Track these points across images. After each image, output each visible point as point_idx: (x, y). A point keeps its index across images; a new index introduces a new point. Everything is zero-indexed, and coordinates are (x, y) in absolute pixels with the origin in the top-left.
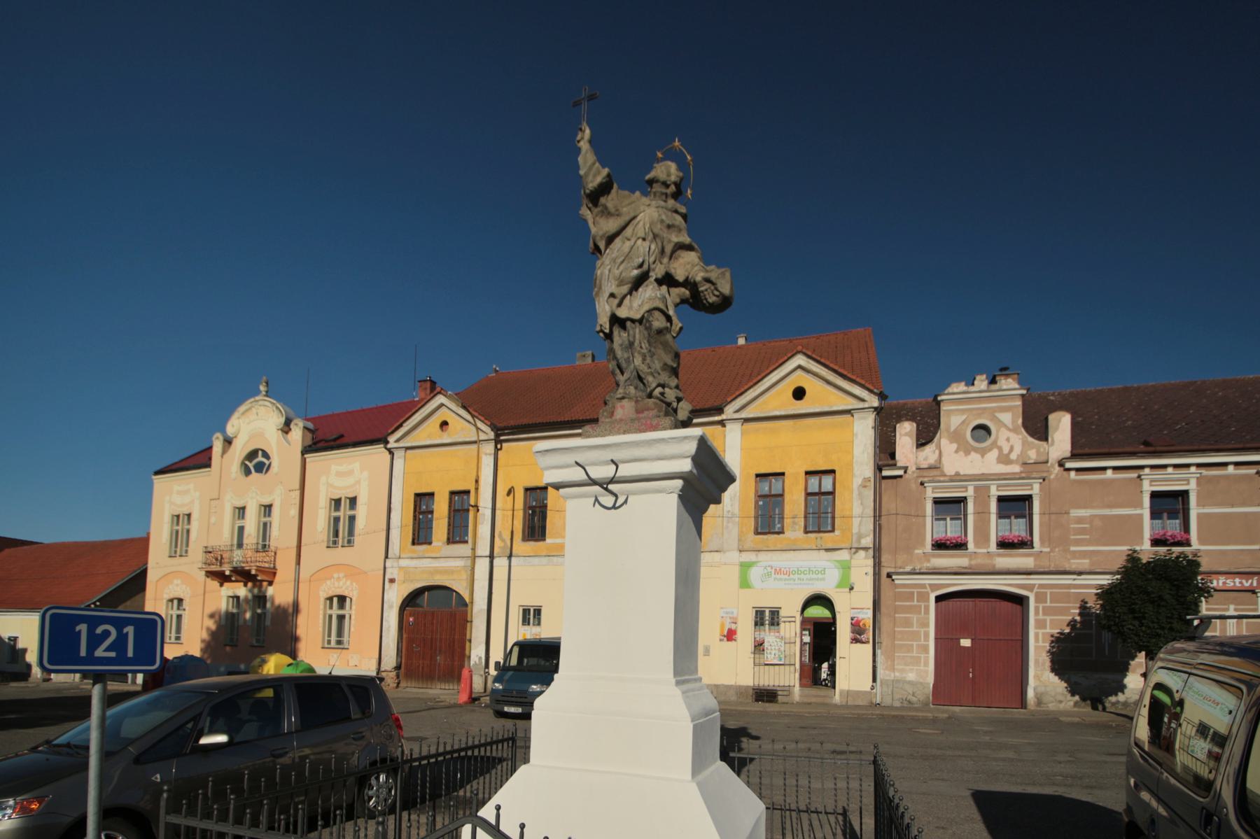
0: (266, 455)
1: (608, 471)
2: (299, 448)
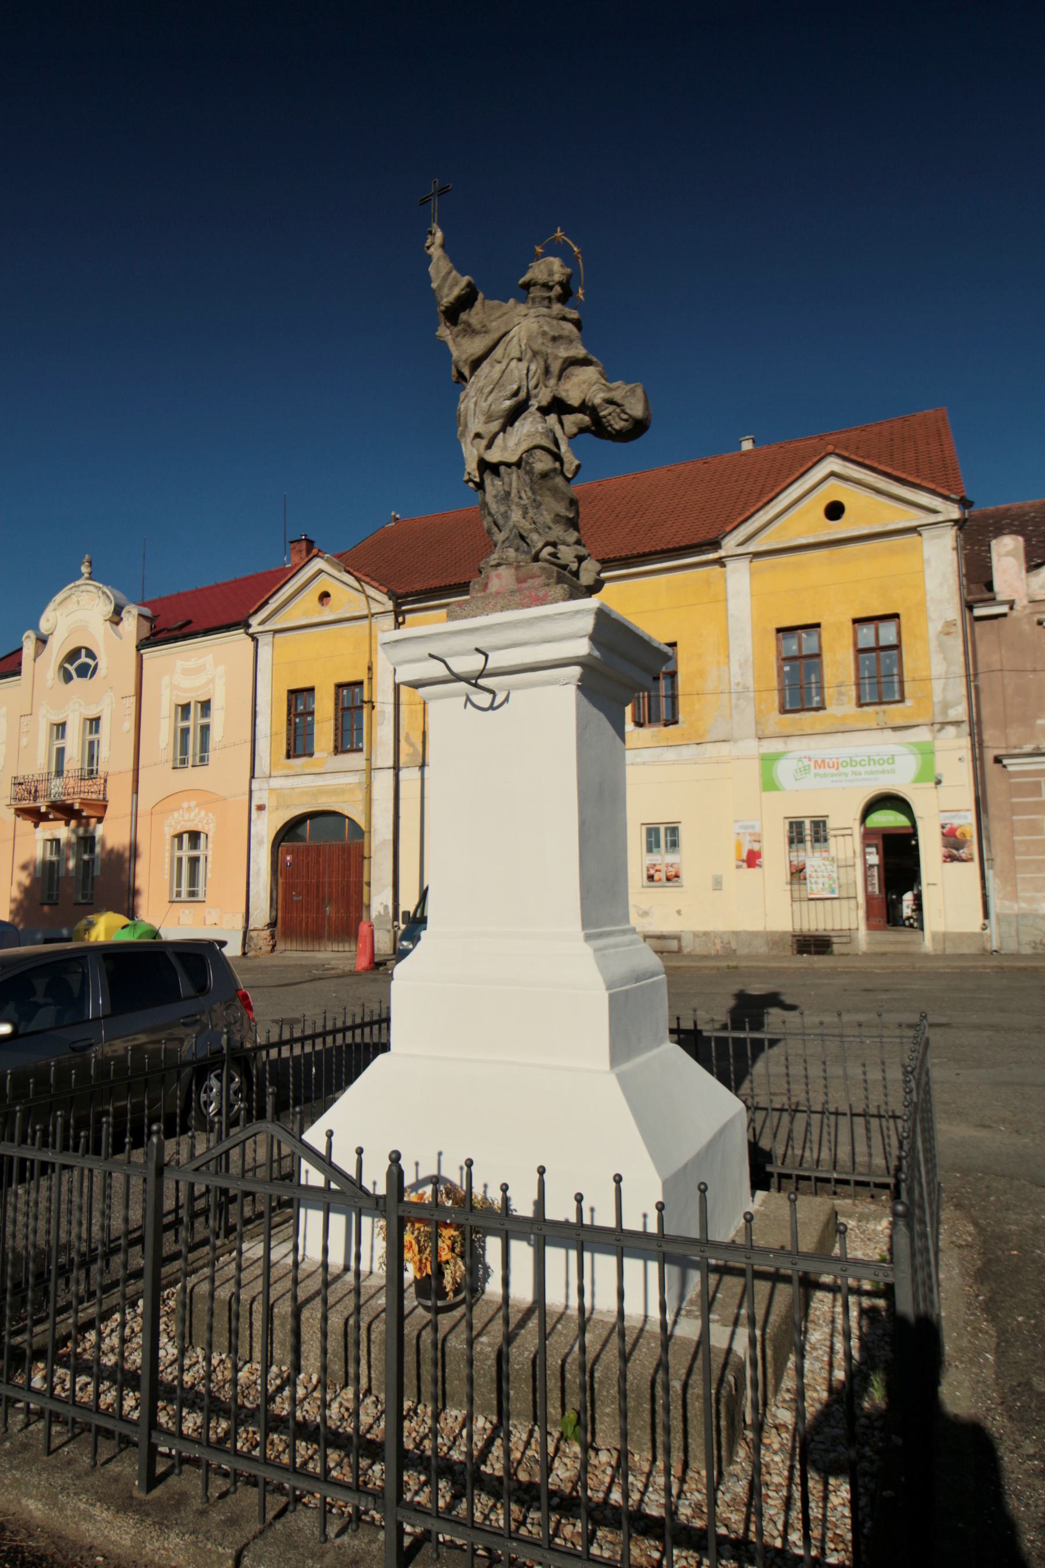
0: (91, 654)
1: (476, 663)
2: (134, 642)
